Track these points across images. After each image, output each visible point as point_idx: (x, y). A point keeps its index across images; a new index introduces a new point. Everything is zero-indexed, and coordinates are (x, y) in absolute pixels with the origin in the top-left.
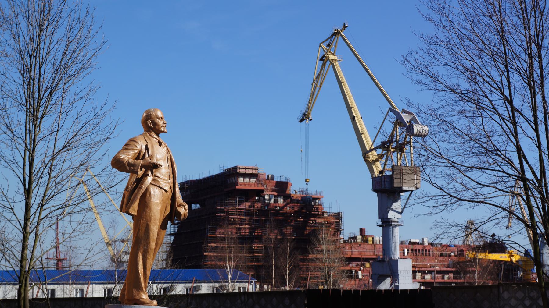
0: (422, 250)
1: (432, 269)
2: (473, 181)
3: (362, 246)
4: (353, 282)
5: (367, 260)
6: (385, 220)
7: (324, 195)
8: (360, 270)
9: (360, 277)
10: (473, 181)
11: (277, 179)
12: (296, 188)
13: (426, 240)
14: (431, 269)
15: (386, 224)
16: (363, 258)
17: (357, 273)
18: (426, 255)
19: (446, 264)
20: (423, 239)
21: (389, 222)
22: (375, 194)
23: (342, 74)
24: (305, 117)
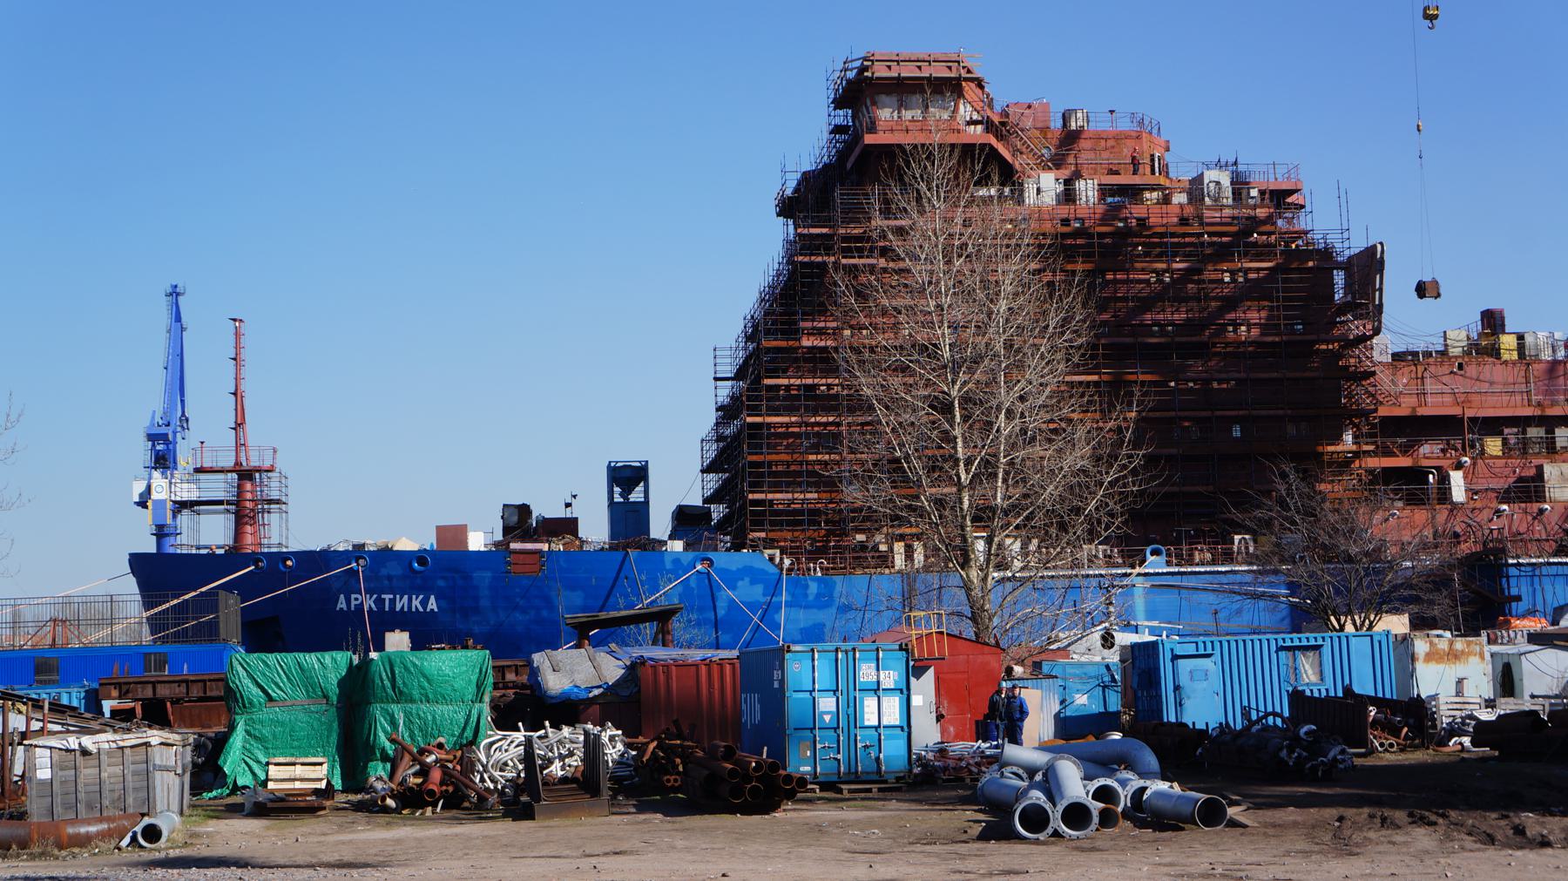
3: (1471, 370)
4: (1421, 515)
5: (1492, 426)
8: (1459, 466)
9: (1458, 493)
16: (1473, 420)
17: (1444, 479)
24: (175, 293)
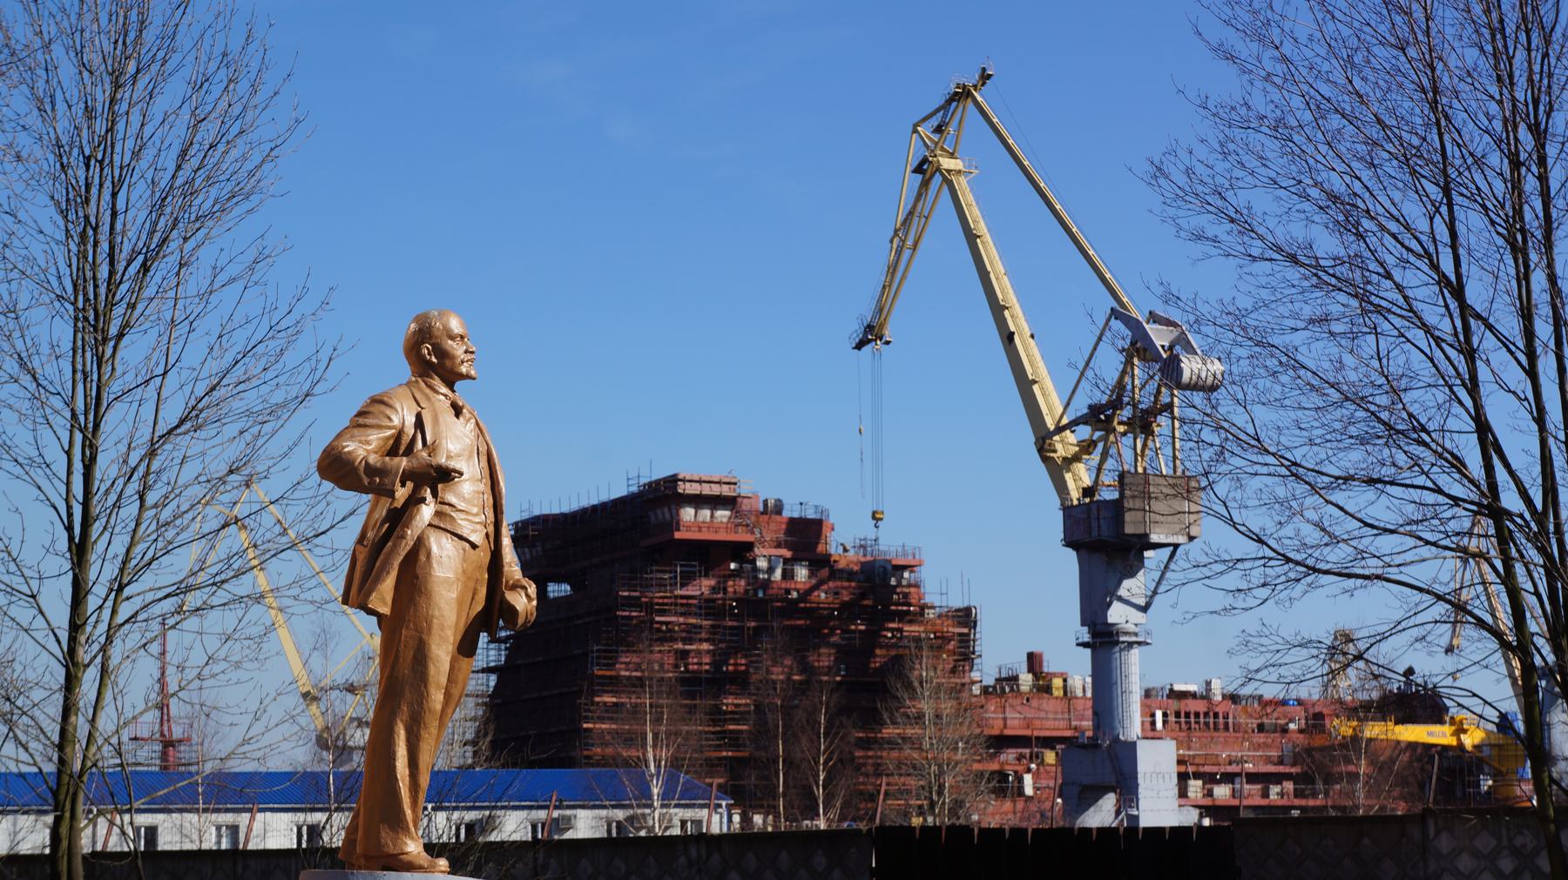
0: (1206, 714)
1: (1234, 768)
2: (1352, 516)
3: (1034, 703)
4: (1008, 805)
5: (1049, 742)
6: (1100, 628)
7: (926, 556)
8: (1029, 771)
9: (1029, 791)
10: (1352, 516)
11: (791, 511)
12: (845, 537)
13: (1217, 686)
14: (1230, 769)
15: (1104, 641)
16: (1038, 738)
17: (1020, 780)
18: (1216, 729)
19: (1274, 753)
20: (1208, 683)
21: (1110, 634)
22: (1071, 554)
23: (976, 212)
